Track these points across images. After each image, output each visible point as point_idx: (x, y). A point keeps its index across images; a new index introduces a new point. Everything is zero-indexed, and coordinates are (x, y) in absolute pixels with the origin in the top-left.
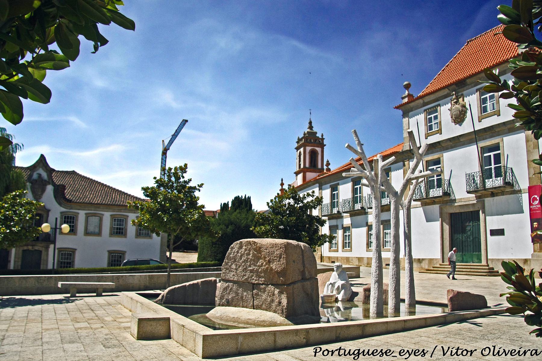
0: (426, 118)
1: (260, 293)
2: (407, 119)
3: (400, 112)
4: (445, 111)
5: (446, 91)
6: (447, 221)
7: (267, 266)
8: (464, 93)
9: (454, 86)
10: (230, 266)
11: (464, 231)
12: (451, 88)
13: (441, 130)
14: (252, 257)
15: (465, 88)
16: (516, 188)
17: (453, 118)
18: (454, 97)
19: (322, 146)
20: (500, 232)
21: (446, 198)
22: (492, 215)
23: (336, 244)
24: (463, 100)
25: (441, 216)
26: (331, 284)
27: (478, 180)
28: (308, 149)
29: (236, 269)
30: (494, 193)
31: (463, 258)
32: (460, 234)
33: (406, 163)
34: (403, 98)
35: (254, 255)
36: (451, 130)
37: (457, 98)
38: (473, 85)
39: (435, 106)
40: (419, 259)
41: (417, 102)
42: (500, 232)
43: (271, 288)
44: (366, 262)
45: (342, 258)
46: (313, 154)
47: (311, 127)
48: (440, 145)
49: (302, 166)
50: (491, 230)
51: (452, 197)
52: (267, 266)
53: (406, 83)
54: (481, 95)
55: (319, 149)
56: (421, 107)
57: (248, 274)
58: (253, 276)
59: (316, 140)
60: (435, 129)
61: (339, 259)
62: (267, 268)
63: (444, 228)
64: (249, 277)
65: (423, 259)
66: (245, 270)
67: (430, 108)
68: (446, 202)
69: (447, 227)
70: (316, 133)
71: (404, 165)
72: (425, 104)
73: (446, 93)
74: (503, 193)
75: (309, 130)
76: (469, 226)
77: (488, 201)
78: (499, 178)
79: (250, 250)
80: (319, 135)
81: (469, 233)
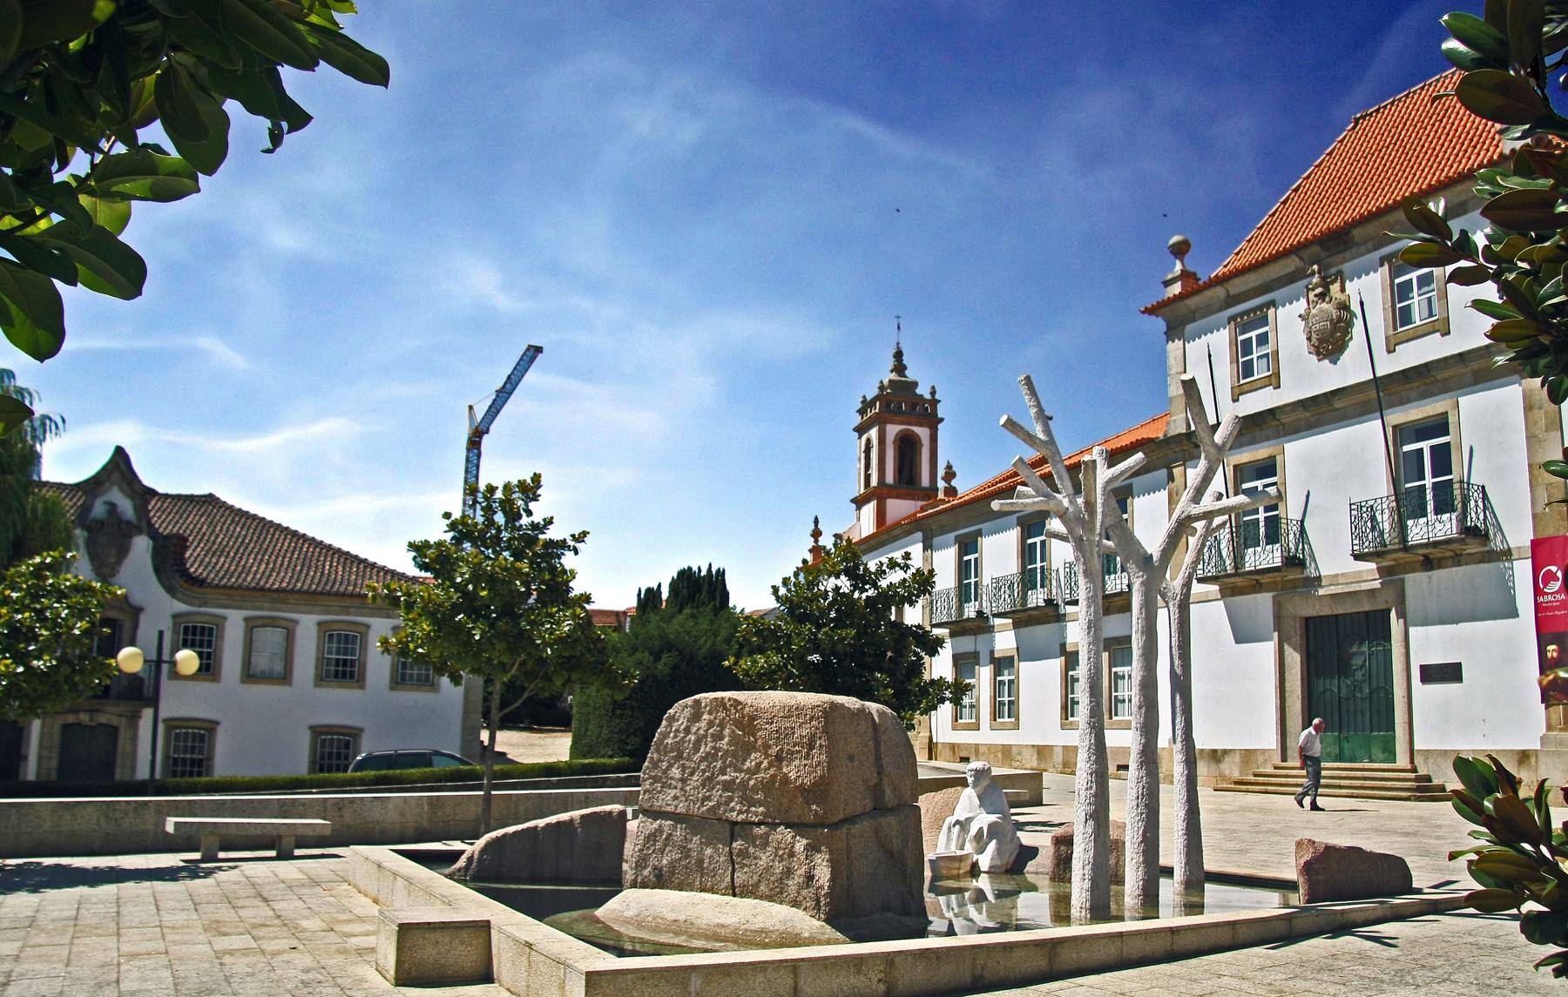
1: (751, 850)
2: (1178, 343)
3: (1159, 324)
4: (1290, 322)
5: (1292, 263)
6: (1297, 639)
7: (772, 771)
8: (1347, 267)
9: (1315, 249)
10: (665, 771)
11: (1344, 669)
12: (1306, 254)
15: (1348, 254)
16: (1497, 544)
17: (1314, 340)
18: (1316, 279)
19: (933, 422)
20: (1449, 673)
21: (1294, 575)
23: (972, 706)
24: (1343, 290)
25: (1278, 625)
26: (958, 822)
27: (1385, 522)
28: (893, 430)
29: (683, 781)
30: (1432, 557)
31: (1341, 749)
32: (1332, 677)
33: (1177, 471)
34: (1167, 284)
35: (734, 739)
38: (1370, 245)
39: (1260, 307)
40: (1215, 751)
42: (1449, 673)
43: (784, 834)
46: (907, 446)
47: (900, 368)
48: (1275, 418)
49: (874, 482)
50: (1423, 668)
51: (1311, 572)
52: (772, 771)
53: (1175, 239)
54: (1395, 273)
55: (923, 432)
56: (1221, 310)
57: (716, 794)
58: (731, 799)
59: (913, 406)
60: (1260, 372)
61: (982, 750)
63: (1288, 661)
64: (719, 804)
65: (1225, 752)
66: (709, 782)
67: (1247, 312)
68: (1293, 586)
69: (1294, 659)
70: (915, 384)
71: (1171, 478)
72: (1232, 301)
73: (1292, 268)
74: (1457, 560)
75: (893, 376)
76: (1361, 653)
77: (1416, 582)
78: (1445, 517)
79: (722, 725)
80: (923, 391)
81: (1359, 675)
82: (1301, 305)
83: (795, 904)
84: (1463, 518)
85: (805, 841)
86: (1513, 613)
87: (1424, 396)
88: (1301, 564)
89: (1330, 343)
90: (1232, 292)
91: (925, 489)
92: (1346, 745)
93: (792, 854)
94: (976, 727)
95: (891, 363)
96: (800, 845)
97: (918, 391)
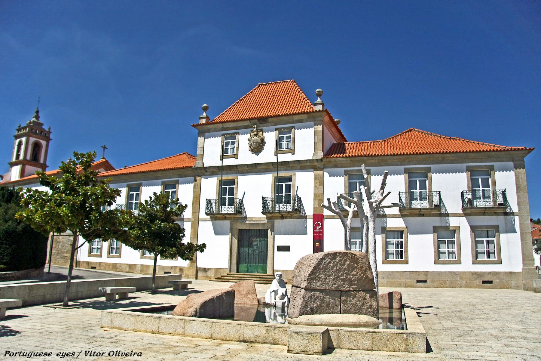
0: (223, 141)
1: (349, 299)
2: (202, 138)
3: (197, 131)
4: (244, 141)
5: (247, 123)
6: (237, 235)
7: (362, 275)
8: (264, 128)
9: (256, 121)
10: (318, 276)
11: (250, 245)
12: (252, 121)
13: (238, 155)
14: (347, 267)
15: (265, 124)
16: (303, 214)
17: (252, 147)
18: (255, 130)
19: (48, 140)
20: (286, 248)
21: (238, 216)
22: (280, 234)
23: (98, 248)
24: (263, 135)
25: (231, 230)
26: (274, 291)
27: (270, 203)
28: (32, 140)
29: (325, 279)
30: (283, 216)
31: (248, 269)
32: (246, 247)
33: (198, 179)
34: (201, 118)
35: (349, 265)
36: (246, 157)
37: (258, 131)
38: (273, 124)
39: (234, 133)
40: (205, 268)
41: (216, 125)
42: (286, 248)
43: (362, 293)
44: (140, 269)
45: (106, 264)
46: (37, 147)
47: (37, 117)
48: (237, 168)
49: (21, 157)
50: (278, 247)
51: (244, 215)
52: (362, 275)
53: (205, 105)
54: (279, 134)
55: (44, 143)
56: (219, 131)
57: (338, 283)
58: (344, 284)
59: (41, 133)
60: (230, 153)
61: (102, 264)
62: (363, 276)
63: (233, 242)
64: (339, 286)
65: (209, 269)
66: (336, 279)
67: (229, 134)
68: (238, 219)
69: (235, 241)
70: (42, 124)
71: (195, 180)
72: (223, 129)
73: (247, 124)
74: (291, 217)
75: (34, 119)
76: (256, 241)
77: (278, 223)
78: (288, 205)
79: (345, 261)
80: (46, 127)
81: (255, 248)
82: (248, 136)
83: (365, 314)
84: (294, 206)
85: (369, 295)
86: (305, 233)
87: (285, 170)
88: (241, 213)
89: (257, 149)
90: (224, 127)
91: (41, 164)
92: (250, 268)
93: (365, 299)
94: (100, 256)
95: (34, 115)
96: (368, 296)
97: (44, 127)
